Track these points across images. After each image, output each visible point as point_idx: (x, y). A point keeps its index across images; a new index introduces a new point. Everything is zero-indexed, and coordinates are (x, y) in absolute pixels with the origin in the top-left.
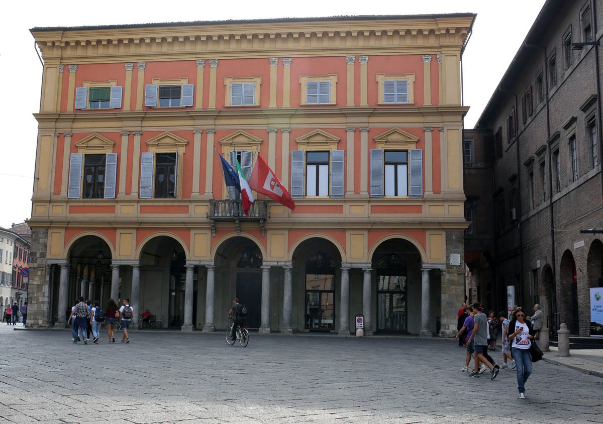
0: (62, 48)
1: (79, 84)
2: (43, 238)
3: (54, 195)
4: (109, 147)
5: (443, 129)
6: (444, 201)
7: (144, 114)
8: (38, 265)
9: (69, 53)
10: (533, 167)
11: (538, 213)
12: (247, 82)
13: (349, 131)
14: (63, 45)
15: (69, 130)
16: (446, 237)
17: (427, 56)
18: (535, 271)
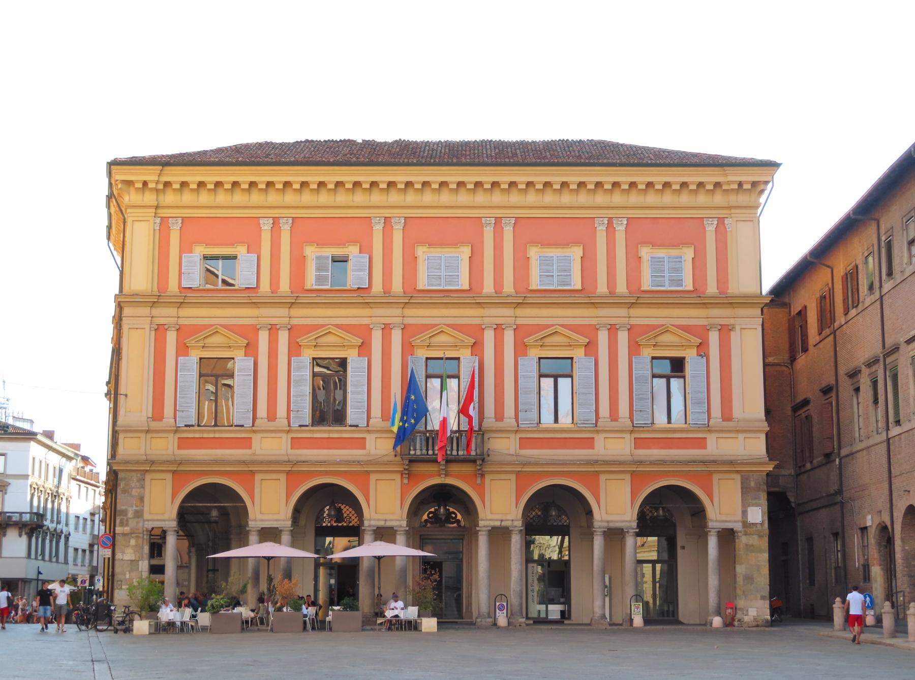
0: (157, 191)
1: (186, 248)
2: (137, 488)
3: (153, 420)
4: (238, 347)
5: (735, 328)
6: (737, 431)
7: (523, 298)
8: (131, 529)
9: (169, 198)
10: (859, 381)
11: (868, 447)
12: (674, 252)
13: (601, 329)
14: (161, 187)
15: (173, 320)
16: (742, 483)
17: (710, 220)
18: (864, 529)
